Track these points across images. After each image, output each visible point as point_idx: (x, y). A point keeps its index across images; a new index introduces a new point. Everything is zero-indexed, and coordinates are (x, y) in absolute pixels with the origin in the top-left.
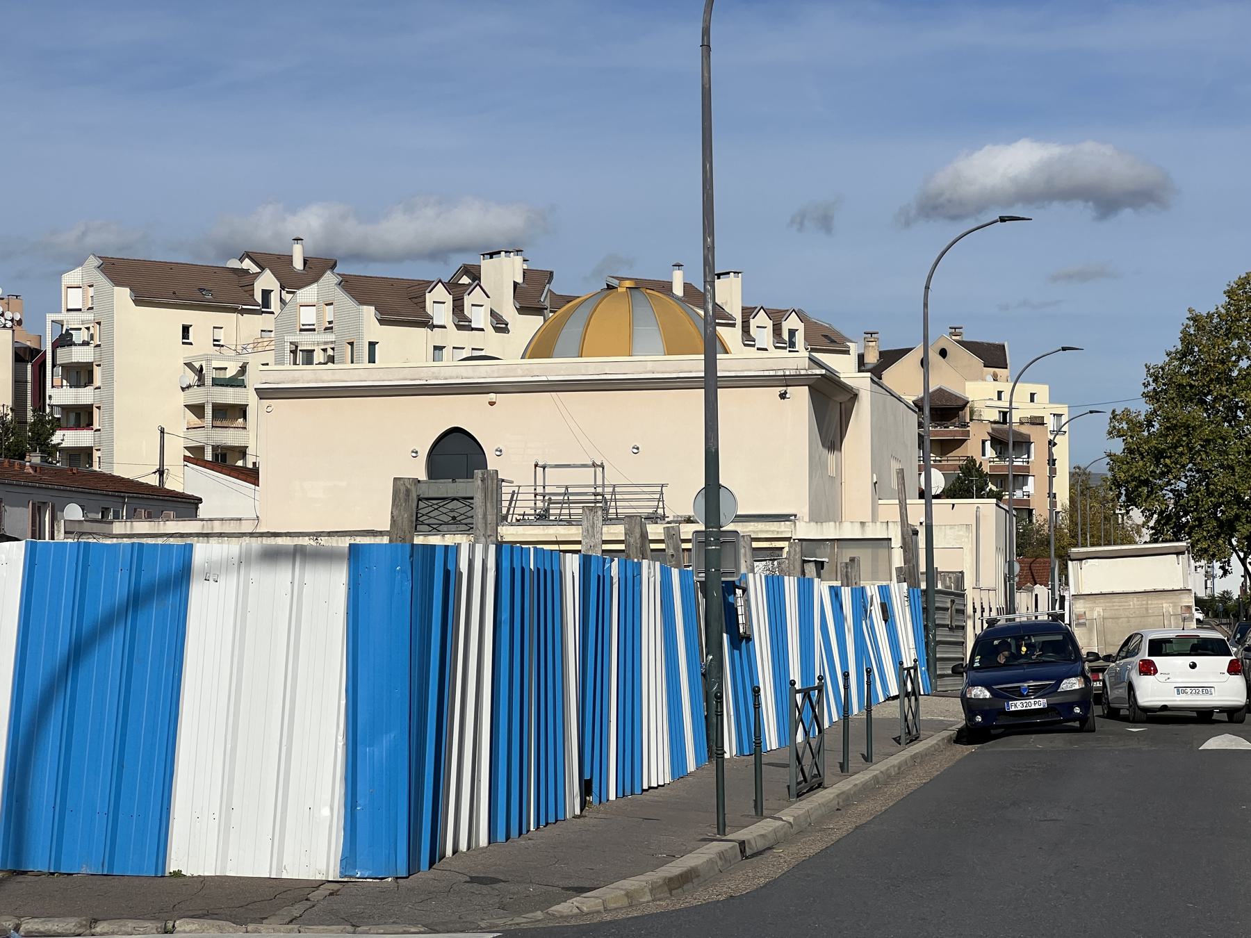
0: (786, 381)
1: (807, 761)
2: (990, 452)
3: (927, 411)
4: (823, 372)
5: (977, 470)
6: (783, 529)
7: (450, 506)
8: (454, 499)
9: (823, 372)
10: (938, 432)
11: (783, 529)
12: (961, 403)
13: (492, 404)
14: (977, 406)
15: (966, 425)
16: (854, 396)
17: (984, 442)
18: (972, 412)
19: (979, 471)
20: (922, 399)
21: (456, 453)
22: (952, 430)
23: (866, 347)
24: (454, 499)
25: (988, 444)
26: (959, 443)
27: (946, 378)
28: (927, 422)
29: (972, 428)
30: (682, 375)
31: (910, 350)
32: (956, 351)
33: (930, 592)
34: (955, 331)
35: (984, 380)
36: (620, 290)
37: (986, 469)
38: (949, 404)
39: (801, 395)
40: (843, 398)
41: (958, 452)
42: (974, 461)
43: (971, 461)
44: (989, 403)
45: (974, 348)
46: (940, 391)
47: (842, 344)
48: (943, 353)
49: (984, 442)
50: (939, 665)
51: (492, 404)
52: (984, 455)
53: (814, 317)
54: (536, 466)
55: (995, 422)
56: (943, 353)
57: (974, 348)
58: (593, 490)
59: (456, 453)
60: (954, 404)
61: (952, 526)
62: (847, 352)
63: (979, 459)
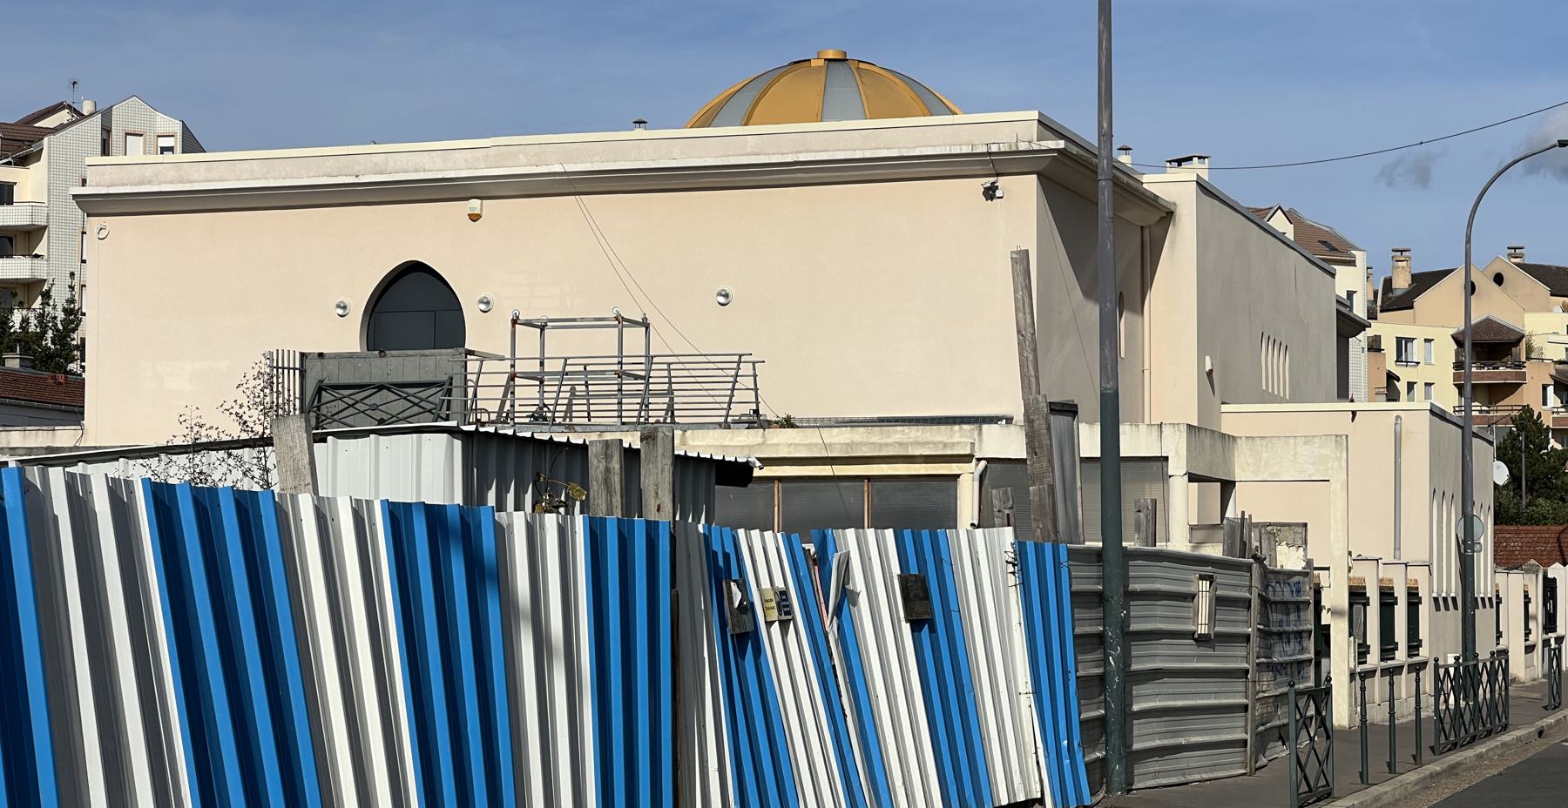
0: (992, 166)
1: (1312, 770)
2: (1553, 400)
3: (1468, 345)
4: (1061, 144)
5: (1535, 422)
6: (958, 439)
7: (377, 399)
8: (381, 387)
9: (1061, 144)
10: (1482, 374)
11: (958, 439)
12: (1514, 338)
13: (474, 218)
14: (1536, 343)
15: (1521, 365)
16: (1167, 215)
17: (1545, 388)
18: (1529, 349)
19: (1537, 424)
20: (1463, 332)
21: (413, 305)
22: (1501, 373)
23: (1394, 268)
24: (381, 387)
25: (1551, 390)
26: (1512, 388)
27: (1494, 307)
28: (1467, 359)
29: (1529, 369)
30: (802, 158)
31: (1450, 271)
32: (1514, 275)
33: (1111, 556)
34: (1515, 251)
35: (1550, 311)
36: (814, 63)
37: (1547, 421)
38: (1498, 338)
39: (1023, 190)
40: (1136, 215)
41: (1511, 400)
42: (1531, 411)
43: (1527, 410)
44: (1552, 338)
45: (1539, 272)
46: (1488, 323)
47: (1346, 252)
48: (1499, 279)
49: (1545, 388)
50: (1139, 728)
51: (474, 218)
52: (1545, 403)
53: (1310, 216)
54: (514, 322)
55: (1561, 362)
56: (1499, 279)
57: (1539, 272)
58: (616, 367)
59: (413, 305)
60: (1506, 338)
61: (1308, 439)
62: (1352, 263)
63: (1537, 408)
